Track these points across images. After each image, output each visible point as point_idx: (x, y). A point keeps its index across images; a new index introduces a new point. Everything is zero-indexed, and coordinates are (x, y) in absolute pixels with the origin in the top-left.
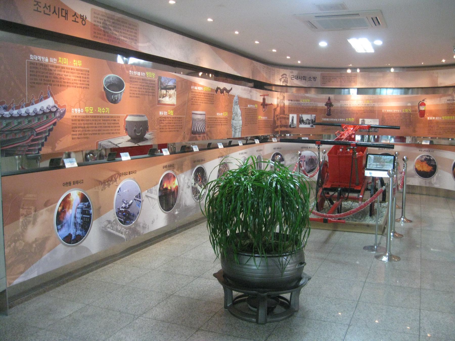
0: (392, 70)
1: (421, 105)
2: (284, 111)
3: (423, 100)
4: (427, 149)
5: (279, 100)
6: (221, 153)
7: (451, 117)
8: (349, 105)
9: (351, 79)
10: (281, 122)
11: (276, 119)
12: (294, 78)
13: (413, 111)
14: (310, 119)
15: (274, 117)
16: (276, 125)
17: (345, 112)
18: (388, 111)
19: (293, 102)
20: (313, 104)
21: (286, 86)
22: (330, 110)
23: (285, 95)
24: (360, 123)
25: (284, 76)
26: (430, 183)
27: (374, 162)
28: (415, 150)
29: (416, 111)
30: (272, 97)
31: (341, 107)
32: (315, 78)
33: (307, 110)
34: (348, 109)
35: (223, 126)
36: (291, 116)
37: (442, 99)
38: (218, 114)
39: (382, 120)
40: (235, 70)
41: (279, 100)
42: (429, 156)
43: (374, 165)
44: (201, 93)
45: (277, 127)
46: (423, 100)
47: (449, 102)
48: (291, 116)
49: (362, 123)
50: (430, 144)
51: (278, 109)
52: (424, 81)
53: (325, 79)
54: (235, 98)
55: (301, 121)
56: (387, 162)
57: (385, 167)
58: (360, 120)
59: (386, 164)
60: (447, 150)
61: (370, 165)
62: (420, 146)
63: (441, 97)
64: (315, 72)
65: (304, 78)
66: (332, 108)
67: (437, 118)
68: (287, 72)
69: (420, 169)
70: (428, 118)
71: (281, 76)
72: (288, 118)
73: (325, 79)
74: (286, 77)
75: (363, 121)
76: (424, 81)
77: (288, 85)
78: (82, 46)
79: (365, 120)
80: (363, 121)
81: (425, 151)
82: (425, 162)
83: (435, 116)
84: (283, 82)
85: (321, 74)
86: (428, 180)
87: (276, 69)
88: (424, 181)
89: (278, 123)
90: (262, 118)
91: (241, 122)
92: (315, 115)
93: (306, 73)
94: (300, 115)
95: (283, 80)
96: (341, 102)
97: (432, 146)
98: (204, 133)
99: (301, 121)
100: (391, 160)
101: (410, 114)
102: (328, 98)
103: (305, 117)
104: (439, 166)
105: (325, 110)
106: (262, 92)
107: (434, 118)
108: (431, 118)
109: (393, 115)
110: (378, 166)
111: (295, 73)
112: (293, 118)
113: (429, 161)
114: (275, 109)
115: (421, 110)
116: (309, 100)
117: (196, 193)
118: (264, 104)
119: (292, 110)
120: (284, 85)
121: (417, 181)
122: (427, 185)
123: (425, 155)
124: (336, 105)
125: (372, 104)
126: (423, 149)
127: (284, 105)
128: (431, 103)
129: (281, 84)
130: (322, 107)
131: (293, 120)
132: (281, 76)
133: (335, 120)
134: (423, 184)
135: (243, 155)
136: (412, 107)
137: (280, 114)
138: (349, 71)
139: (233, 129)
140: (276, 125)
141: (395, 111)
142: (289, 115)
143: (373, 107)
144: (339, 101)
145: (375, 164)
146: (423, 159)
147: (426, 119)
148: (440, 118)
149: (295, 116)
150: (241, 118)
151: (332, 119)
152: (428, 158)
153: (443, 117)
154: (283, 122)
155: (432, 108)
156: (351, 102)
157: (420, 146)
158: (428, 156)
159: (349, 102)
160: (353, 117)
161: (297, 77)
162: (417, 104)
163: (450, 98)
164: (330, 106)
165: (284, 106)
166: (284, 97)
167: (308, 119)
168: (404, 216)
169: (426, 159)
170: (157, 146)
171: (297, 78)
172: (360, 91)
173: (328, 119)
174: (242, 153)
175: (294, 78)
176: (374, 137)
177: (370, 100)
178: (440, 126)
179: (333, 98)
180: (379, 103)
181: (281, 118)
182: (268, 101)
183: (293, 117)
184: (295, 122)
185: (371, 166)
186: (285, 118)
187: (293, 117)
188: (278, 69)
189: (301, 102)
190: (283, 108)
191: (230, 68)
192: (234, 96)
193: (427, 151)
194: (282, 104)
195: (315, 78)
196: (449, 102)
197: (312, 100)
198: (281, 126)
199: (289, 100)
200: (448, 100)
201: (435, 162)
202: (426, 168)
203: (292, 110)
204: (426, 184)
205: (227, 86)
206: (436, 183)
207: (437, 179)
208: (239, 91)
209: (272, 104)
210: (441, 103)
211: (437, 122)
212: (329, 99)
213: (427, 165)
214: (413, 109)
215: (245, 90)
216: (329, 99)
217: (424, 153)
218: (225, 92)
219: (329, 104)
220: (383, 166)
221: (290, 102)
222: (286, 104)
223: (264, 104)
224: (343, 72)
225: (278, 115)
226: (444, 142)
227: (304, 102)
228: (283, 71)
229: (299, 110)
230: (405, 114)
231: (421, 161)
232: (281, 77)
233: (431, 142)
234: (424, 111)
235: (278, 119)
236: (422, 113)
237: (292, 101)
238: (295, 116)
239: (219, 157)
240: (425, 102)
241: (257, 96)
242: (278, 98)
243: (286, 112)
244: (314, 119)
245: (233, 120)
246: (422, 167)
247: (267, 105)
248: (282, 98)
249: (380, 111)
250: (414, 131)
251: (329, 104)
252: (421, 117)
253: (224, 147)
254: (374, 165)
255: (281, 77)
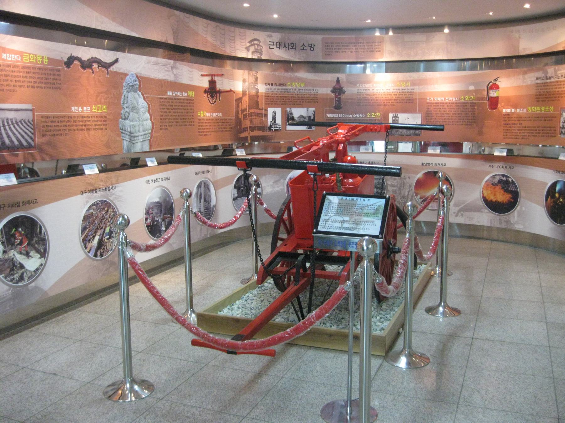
0: (446, 31)
1: (492, 88)
2: (257, 103)
3: (496, 80)
4: (501, 164)
5: (247, 84)
6: (90, 184)
7: (543, 108)
8: (371, 91)
9: (373, 47)
10: (251, 121)
11: (241, 116)
12: (274, 47)
13: (478, 99)
14: (305, 115)
15: (237, 113)
16: (243, 127)
17: (365, 102)
18: (436, 99)
19: (274, 87)
20: (310, 90)
21: (259, 60)
22: (340, 98)
23: (259, 75)
24: (391, 121)
25: (256, 42)
26: (508, 222)
27: (337, 214)
28: (480, 166)
29: (483, 99)
30: (232, 78)
31: (358, 94)
32: (312, 47)
33: (300, 101)
34: (369, 97)
35: (92, 132)
36: (271, 111)
37: (526, 76)
38: (74, 109)
39: (427, 116)
40: (114, 19)
41: (247, 84)
42: (507, 177)
43: (335, 221)
44: (17, 67)
45: (245, 130)
46: (496, 80)
47: (539, 81)
48: (271, 111)
49: (394, 122)
50: (507, 155)
51: (246, 99)
52: (495, 46)
53: (328, 47)
54: (129, 79)
55: (289, 119)
56: (367, 215)
57: (361, 226)
58: (391, 115)
59: (365, 219)
60: (534, 166)
61: (327, 221)
62: (490, 158)
63: (525, 73)
64: (312, 36)
65: (292, 46)
66: (343, 97)
67: (518, 110)
68: (261, 35)
69: (492, 198)
70: (504, 111)
71: (249, 42)
72: (266, 115)
73: (328, 47)
74: (258, 45)
75: (396, 117)
76: (495, 46)
77: (263, 57)
78: (109, 32)
79: (399, 115)
80: (396, 117)
81: (499, 166)
82: (500, 186)
83: (515, 107)
84: (253, 52)
85: (323, 39)
86: (504, 216)
87: (238, 30)
88: (498, 218)
89: (247, 123)
90: (207, 115)
91: (149, 123)
92: (314, 109)
93: (295, 37)
94: (288, 109)
95: (252, 49)
96: (358, 85)
97: (511, 157)
98: (30, 147)
99: (289, 119)
100: (377, 210)
101: (473, 104)
102: (336, 79)
103: (298, 112)
104: (522, 194)
105: (331, 99)
106: (206, 69)
107: (513, 110)
108: (509, 111)
109: (445, 107)
110: (346, 225)
111: (276, 37)
112: (275, 114)
113: (506, 184)
114: (239, 100)
115: (492, 97)
116: (303, 84)
117: (12, 270)
118: (212, 90)
119: (272, 100)
120: (255, 57)
121: (485, 218)
122: (503, 226)
123: (498, 175)
124: (350, 91)
125: (410, 88)
126: (496, 164)
127: (257, 92)
128: (509, 84)
129: (250, 56)
130: (327, 94)
131: (274, 118)
132: (249, 42)
133: (348, 116)
134: (497, 224)
135: (157, 184)
136: (476, 91)
137: (250, 108)
138: (377, 34)
139: (126, 137)
140: (243, 127)
141: (448, 99)
142: (266, 110)
143: (411, 93)
144: (356, 85)
145: (339, 218)
146: (496, 181)
147: (501, 112)
148: (525, 110)
149: (279, 111)
150: (148, 115)
151: (344, 115)
152: (505, 179)
153: (529, 108)
154: (257, 122)
155: (512, 93)
156: (375, 85)
157: (490, 158)
158: (503, 176)
159: (371, 85)
160: (379, 112)
161: (280, 45)
162: (485, 88)
163: (540, 74)
164: (340, 94)
165: (257, 95)
166: (256, 79)
167: (302, 116)
168: (445, 302)
169: (500, 182)
170: (130, 160)
171: (280, 45)
172: (392, 66)
173: (337, 116)
174: (154, 181)
175: (274, 47)
176: (421, 143)
177: (407, 81)
178: (525, 124)
179: (345, 79)
180: (421, 87)
181: (251, 115)
182: (222, 84)
183: (275, 113)
184: (279, 121)
185: (329, 224)
186: (259, 115)
187: (275, 113)
188: (242, 30)
189: (289, 87)
190: (255, 100)
191: (106, 20)
192: (126, 75)
193: (503, 167)
194: (253, 92)
195: (312, 47)
196: (539, 81)
197: (308, 83)
198: (252, 129)
199: (266, 84)
200: (537, 79)
201: (516, 187)
202: (501, 197)
203: (272, 100)
204: (500, 223)
205: (106, 56)
206: (517, 223)
207: (519, 214)
208: (133, 64)
209: (231, 91)
210: (524, 84)
211: (519, 118)
212: (338, 81)
213: (502, 191)
214: (479, 95)
215: (156, 63)
216: (338, 81)
217: (496, 171)
218: (95, 66)
219: (338, 90)
220: (357, 223)
221: (268, 87)
222: (259, 91)
223: (212, 90)
224: (366, 34)
225: (245, 110)
226: (529, 151)
227: (294, 87)
228: (251, 34)
229: (286, 100)
230: (465, 104)
231: (492, 185)
232: (248, 44)
233: (510, 151)
234: (497, 98)
235: (245, 116)
236: (494, 103)
237: (272, 85)
238: (279, 111)
239: (82, 193)
240: (498, 83)
241: (195, 76)
242: (244, 81)
243: (262, 104)
244: (312, 116)
245: (125, 119)
246: (495, 195)
247: (220, 92)
248: (252, 80)
249: (423, 101)
250: (480, 133)
251: (338, 90)
252: (492, 109)
253: (159, 164)
254: (335, 221)
255: (248, 44)
